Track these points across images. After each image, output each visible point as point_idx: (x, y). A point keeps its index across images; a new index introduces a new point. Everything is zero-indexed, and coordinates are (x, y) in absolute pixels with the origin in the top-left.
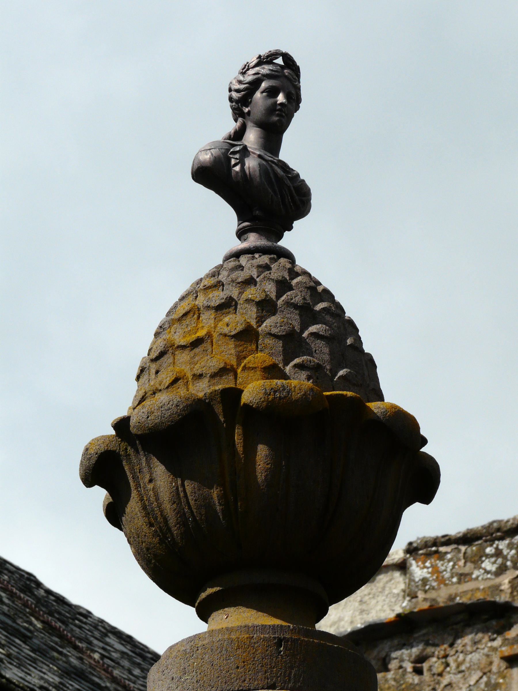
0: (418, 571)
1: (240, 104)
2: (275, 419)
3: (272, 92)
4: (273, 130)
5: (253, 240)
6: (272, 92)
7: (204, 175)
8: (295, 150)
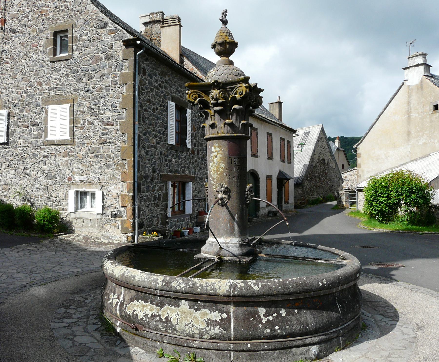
0: (151, 16)
1: (223, 14)
2: (229, 43)
3: (225, 13)
4: (225, 16)
5: (224, 26)
6: (225, 13)
7: (220, 20)
8: (227, 18)
